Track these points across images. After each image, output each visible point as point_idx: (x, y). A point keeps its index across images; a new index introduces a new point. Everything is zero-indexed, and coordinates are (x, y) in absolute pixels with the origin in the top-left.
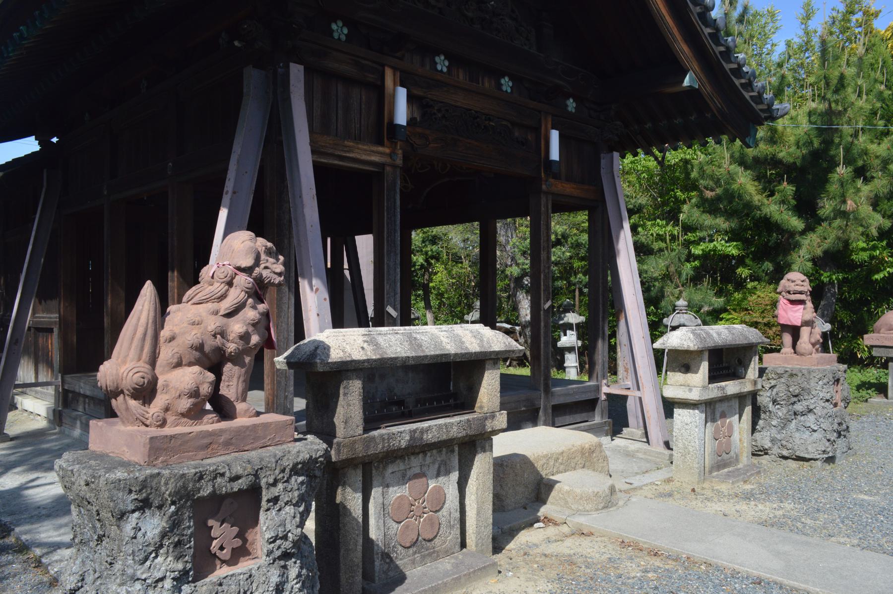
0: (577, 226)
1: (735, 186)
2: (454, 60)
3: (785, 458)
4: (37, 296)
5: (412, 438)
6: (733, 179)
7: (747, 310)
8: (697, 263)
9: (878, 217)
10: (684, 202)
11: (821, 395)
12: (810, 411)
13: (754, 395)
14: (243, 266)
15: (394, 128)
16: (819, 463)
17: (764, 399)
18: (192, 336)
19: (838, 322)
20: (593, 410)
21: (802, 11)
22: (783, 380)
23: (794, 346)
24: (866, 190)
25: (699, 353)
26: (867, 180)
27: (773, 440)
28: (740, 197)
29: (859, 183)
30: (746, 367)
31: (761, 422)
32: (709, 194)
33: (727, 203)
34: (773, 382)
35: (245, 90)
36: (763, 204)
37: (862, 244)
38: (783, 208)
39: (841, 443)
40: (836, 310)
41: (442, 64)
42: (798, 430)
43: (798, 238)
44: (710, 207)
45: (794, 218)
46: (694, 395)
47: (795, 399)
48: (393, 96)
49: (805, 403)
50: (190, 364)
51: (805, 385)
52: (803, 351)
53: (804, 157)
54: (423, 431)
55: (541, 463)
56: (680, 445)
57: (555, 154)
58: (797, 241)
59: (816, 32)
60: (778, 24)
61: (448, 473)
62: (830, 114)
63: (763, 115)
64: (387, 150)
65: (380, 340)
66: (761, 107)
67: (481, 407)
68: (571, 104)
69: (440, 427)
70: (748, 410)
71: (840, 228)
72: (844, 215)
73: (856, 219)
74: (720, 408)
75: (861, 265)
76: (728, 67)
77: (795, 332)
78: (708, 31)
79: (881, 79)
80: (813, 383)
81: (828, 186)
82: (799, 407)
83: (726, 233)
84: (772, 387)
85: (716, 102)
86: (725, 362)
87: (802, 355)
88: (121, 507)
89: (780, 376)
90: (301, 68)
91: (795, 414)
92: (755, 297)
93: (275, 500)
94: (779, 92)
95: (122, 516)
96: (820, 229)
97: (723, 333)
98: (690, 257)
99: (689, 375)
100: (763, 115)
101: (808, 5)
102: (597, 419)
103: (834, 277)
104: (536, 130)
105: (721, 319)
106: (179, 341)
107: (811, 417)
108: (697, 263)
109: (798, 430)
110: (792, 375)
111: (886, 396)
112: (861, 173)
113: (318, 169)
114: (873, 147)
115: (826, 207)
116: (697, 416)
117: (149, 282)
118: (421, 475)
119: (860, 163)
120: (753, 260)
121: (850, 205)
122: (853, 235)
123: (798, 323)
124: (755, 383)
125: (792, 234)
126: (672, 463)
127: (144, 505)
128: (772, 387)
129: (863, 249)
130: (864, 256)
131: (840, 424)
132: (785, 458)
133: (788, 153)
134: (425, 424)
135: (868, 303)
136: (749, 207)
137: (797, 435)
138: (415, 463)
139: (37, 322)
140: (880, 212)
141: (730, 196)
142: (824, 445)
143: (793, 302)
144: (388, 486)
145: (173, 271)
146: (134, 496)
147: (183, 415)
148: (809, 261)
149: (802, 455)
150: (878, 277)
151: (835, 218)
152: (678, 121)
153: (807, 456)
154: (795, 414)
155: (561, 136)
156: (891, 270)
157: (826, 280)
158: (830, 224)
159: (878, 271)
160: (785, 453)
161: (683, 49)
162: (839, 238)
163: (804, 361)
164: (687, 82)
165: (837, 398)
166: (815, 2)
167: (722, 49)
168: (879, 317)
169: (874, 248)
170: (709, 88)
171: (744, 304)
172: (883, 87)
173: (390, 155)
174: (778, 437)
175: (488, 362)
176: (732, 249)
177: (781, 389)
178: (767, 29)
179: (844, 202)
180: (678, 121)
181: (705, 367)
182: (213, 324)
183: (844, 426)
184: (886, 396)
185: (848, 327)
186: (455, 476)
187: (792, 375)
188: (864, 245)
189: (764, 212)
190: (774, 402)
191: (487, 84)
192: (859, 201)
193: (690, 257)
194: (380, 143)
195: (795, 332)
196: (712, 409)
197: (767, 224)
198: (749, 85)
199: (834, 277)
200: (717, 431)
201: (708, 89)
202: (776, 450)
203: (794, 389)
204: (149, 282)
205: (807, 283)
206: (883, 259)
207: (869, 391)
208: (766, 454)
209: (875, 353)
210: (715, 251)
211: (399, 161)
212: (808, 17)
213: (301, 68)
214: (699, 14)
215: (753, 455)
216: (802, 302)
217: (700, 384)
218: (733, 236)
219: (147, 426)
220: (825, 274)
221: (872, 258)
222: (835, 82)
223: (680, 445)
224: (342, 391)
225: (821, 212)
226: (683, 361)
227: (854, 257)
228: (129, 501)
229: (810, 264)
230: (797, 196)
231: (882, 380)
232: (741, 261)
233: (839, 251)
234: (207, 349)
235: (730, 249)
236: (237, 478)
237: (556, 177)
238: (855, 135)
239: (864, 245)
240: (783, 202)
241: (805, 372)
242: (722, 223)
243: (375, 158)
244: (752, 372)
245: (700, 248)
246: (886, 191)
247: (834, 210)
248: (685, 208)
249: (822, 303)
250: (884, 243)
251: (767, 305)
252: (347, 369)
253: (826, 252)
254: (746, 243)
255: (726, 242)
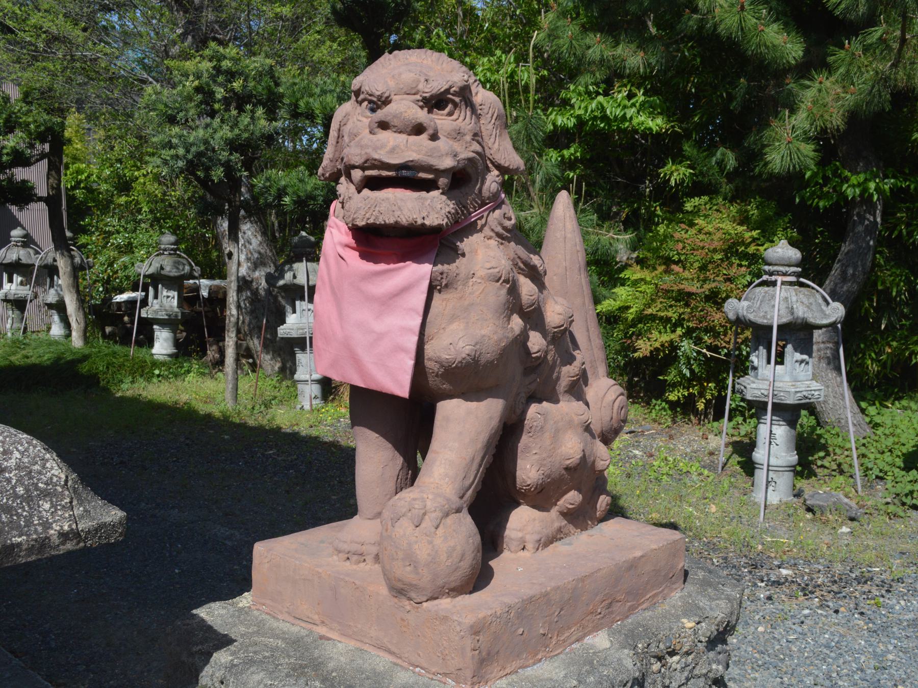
0: (357, 49)
14: (502, 162)
19: (880, 293)
40: (875, 264)
45: (775, 26)
103: (872, 185)
117: (202, 612)
120: (699, 144)
148: (807, 140)
156: (2, 177)
157: (850, 192)
199: (872, 185)
204: (202, 612)
220: (854, 180)
233: (879, 115)
249: (845, 248)
251: (715, 251)
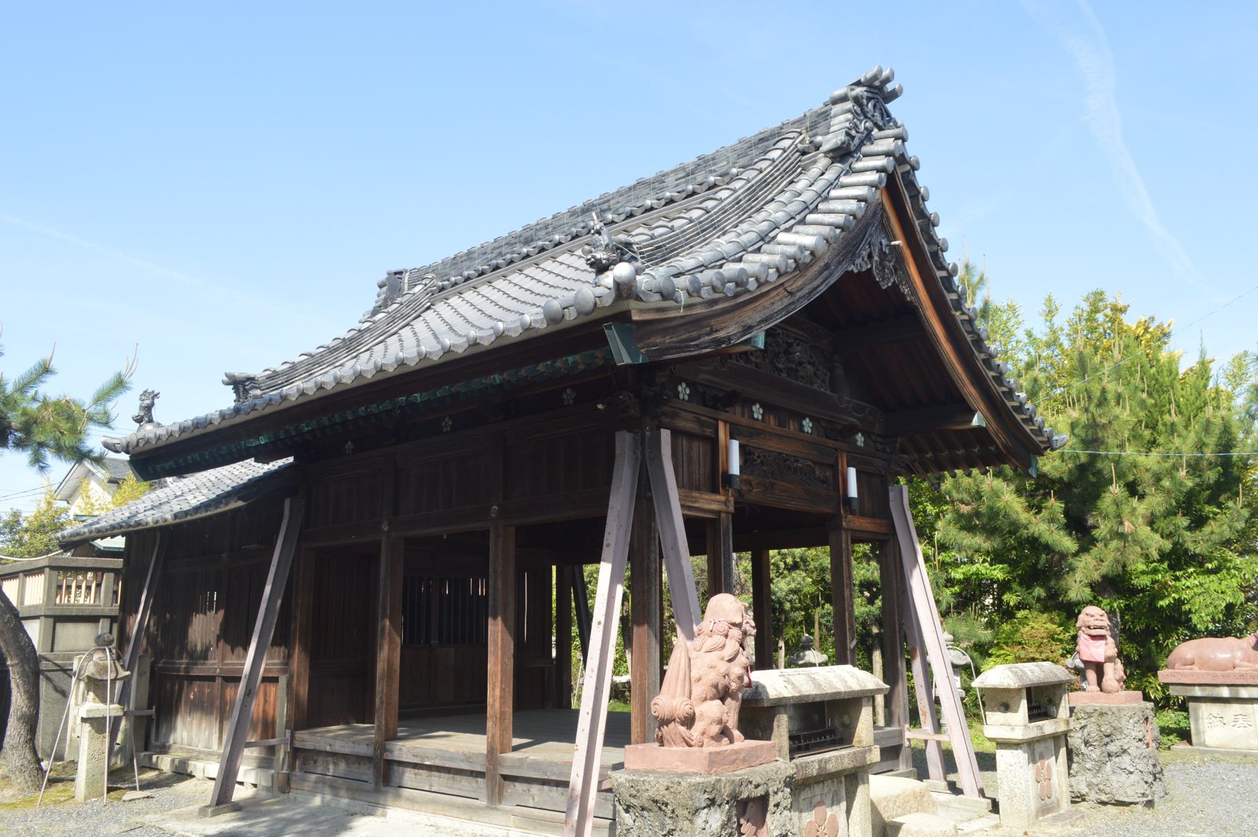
1: (1000, 504)
2: (767, 408)
3: (1104, 803)
4: (300, 642)
5: (820, 768)
6: (998, 497)
7: (1020, 643)
8: (957, 589)
9: (1157, 537)
10: (937, 516)
11: (1134, 734)
12: (1124, 751)
13: (1065, 735)
15: (728, 478)
16: (1139, 807)
17: (1076, 741)
18: (712, 677)
20: (897, 757)
21: (1044, 307)
22: (1093, 719)
23: (1099, 683)
24: (1142, 508)
25: (1019, 690)
26: (1142, 497)
27: (1089, 785)
28: (1006, 515)
29: (1134, 502)
30: (1057, 706)
31: (1074, 766)
32: (965, 509)
33: (986, 521)
34: (1083, 722)
35: (617, 452)
36: (1030, 523)
37: (1141, 567)
38: (1054, 527)
39: (1157, 785)
41: (758, 411)
42: (1114, 772)
43: (1071, 560)
44: (967, 524)
46: (1018, 734)
47: (1107, 740)
48: (727, 448)
49: (1118, 743)
50: (712, 699)
51: (1116, 724)
52: (1109, 688)
53: (1070, 471)
54: (827, 761)
55: (883, 805)
56: (1006, 788)
57: (853, 492)
58: (1071, 564)
59: (1062, 329)
60: (1020, 319)
61: (839, 802)
62: (1093, 425)
63: (1043, 446)
64: (722, 498)
65: (792, 679)
66: (1040, 439)
67: (860, 742)
68: (860, 439)
69: (836, 757)
70: (1063, 751)
71: (1118, 549)
72: (1122, 536)
73: (1134, 541)
74: (1039, 748)
75: (1143, 590)
76: (1009, 404)
77: (1099, 668)
78: (991, 374)
79: (1141, 386)
80: (1124, 722)
81: (1099, 503)
82: (1112, 748)
83: (988, 553)
84: (1083, 728)
85: (1000, 438)
86: (1041, 701)
87: (1109, 692)
88: (697, 805)
89: (1090, 715)
90: (668, 432)
91: (1109, 755)
92: (1027, 628)
93: (777, 805)
94: (1033, 394)
95: (696, 811)
96: (1094, 551)
97: (1038, 672)
98: (950, 582)
99: (1009, 714)
100: (1043, 446)
101: (1049, 300)
102: (902, 768)
104: (834, 467)
105: (990, 655)
106: (704, 680)
107: (1126, 758)
108: (957, 589)
109: (1114, 772)
110: (1102, 714)
111: (1190, 742)
112: (1133, 489)
113: (688, 521)
114: (1142, 459)
115: (1103, 530)
116: (1020, 756)
118: (821, 803)
119: (1131, 478)
120: (1021, 584)
121: (1127, 527)
122: (1132, 557)
123: (1102, 659)
124: (1068, 723)
125: (1063, 556)
126: (995, 807)
127: (712, 803)
128: (1083, 728)
129: (1143, 573)
130: (1145, 581)
131: (1154, 766)
132: (1104, 803)
133: (1053, 467)
134: (827, 755)
135: (1155, 634)
136: (1015, 527)
137: (1114, 778)
138: (818, 790)
139: (228, 670)
140: (1156, 531)
141: (994, 514)
142: (1143, 788)
143: (1094, 637)
144: (801, 812)
145: (495, 618)
146: (706, 796)
147: (712, 738)
149: (1122, 799)
150: (1163, 603)
151: (1112, 539)
152: (961, 452)
153: (1127, 800)
154: (1109, 755)
155: (858, 473)
158: (1106, 545)
159: (1162, 598)
160: (1104, 798)
161: (970, 392)
162: (1117, 561)
163: (1111, 700)
164: (976, 421)
165: (1149, 738)
166: (1058, 300)
167: (1005, 389)
168: (1171, 651)
169: (1155, 571)
170: (994, 425)
171: (1017, 637)
172: (1144, 395)
173: (725, 503)
174: (1095, 781)
175: (782, 710)
176: (998, 572)
177: (1092, 728)
178: (1010, 324)
179: (1121, 523)
180: (961, 452)
181: (1024, 704)
182: (723, 666)
183: (1158, 769)
184: (1190, 742)
185: (1137, 662)
186: (844, 805)
187: (1102, 714)
188: (1144, 567)
189: (1031, 531)
190: (1086, 743)
191: (792, 426)
192: (1134, 524)
193: (950, 582)
194: (715, 491)
195: (1099, 668)
196: (1035, 749)
197: (1035, 544)
198: (1030, 420)
200: (1038, 773)
201: (993, 427)
202: (1093, 796)
203: (1106, 729)
205: (1105, 618)
206: (1166, 583)
207: (1171, 737)
208: (1084, 800)
209: (1172, 691)
210: (977, 574)
211: (732, 509)
212: (1050, 313)
213: (668, 432)
214: (984, 360)
215: (1073, 802)
216: (1102, 637)
217: (1022, 723)
218: (997, 557)
219: (690, 746)
221: (1154, 582)
222: (1098, 394)
223: (1006, 788)
224: (775, 724)
225: (1096, 533)
226: (1002, 700)
227: (1135, 582)
228: (702, 799)
229: (1088, 590)
230: (1066, 513)
231: (1182, 725)
232: (1005, 586)
233: (1119, 576)
234: (720, 687)
235: (995, 573)
236: (757, 786)
237: (853, 513)
238: (1121, 446)
239: (1144, 567)
240: (1052, 520)
241: (1115, 710)
242: (979, 540)
243: (714, 507)
244: (1063, 712)
245: (960, 570)
246: (1162, 509)
247: (1111, 531)
248: (940, 524)
250: (1165, 565)
252: (779, 705)
253: (1104, 577)
254: (1013, 564)
255: (991, 565)
